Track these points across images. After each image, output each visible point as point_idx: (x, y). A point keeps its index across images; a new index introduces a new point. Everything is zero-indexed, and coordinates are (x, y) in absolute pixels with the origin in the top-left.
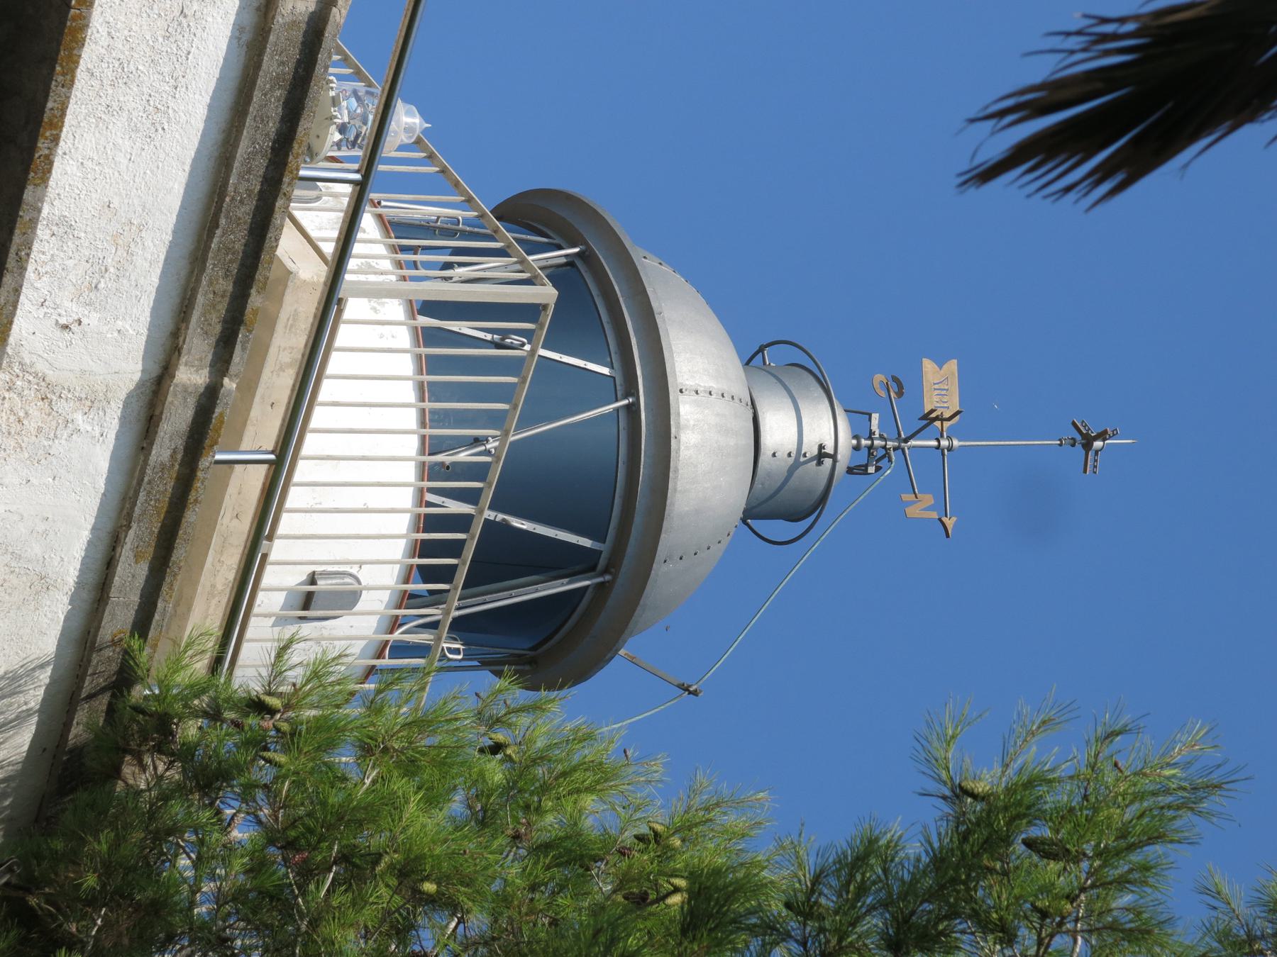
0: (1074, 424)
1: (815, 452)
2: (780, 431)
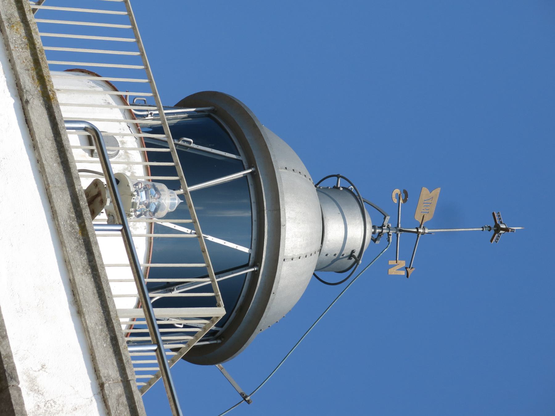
0: (493, 214)
1: (349, 253)
2: (335, 232)
